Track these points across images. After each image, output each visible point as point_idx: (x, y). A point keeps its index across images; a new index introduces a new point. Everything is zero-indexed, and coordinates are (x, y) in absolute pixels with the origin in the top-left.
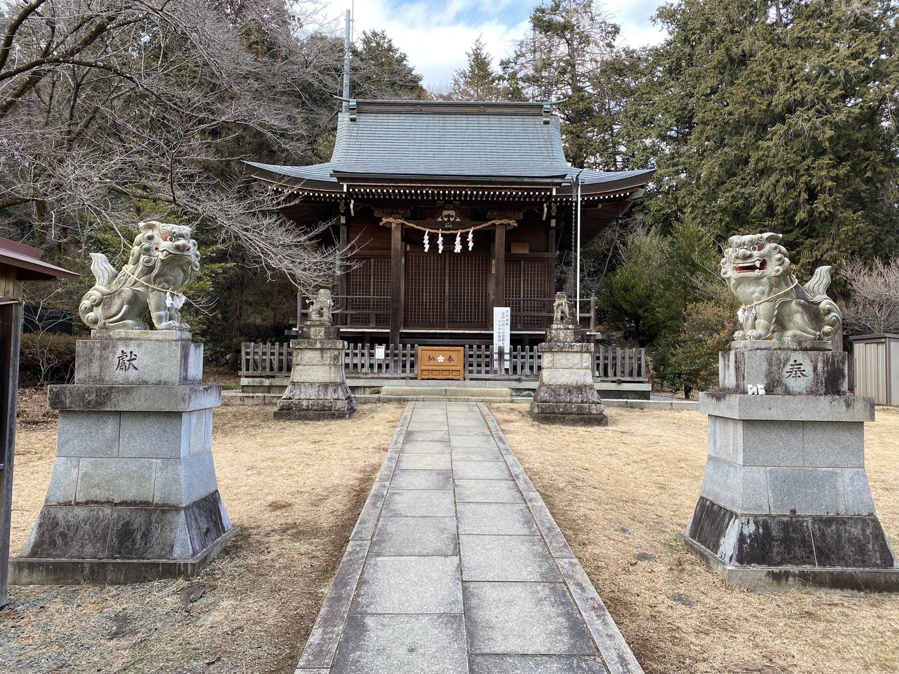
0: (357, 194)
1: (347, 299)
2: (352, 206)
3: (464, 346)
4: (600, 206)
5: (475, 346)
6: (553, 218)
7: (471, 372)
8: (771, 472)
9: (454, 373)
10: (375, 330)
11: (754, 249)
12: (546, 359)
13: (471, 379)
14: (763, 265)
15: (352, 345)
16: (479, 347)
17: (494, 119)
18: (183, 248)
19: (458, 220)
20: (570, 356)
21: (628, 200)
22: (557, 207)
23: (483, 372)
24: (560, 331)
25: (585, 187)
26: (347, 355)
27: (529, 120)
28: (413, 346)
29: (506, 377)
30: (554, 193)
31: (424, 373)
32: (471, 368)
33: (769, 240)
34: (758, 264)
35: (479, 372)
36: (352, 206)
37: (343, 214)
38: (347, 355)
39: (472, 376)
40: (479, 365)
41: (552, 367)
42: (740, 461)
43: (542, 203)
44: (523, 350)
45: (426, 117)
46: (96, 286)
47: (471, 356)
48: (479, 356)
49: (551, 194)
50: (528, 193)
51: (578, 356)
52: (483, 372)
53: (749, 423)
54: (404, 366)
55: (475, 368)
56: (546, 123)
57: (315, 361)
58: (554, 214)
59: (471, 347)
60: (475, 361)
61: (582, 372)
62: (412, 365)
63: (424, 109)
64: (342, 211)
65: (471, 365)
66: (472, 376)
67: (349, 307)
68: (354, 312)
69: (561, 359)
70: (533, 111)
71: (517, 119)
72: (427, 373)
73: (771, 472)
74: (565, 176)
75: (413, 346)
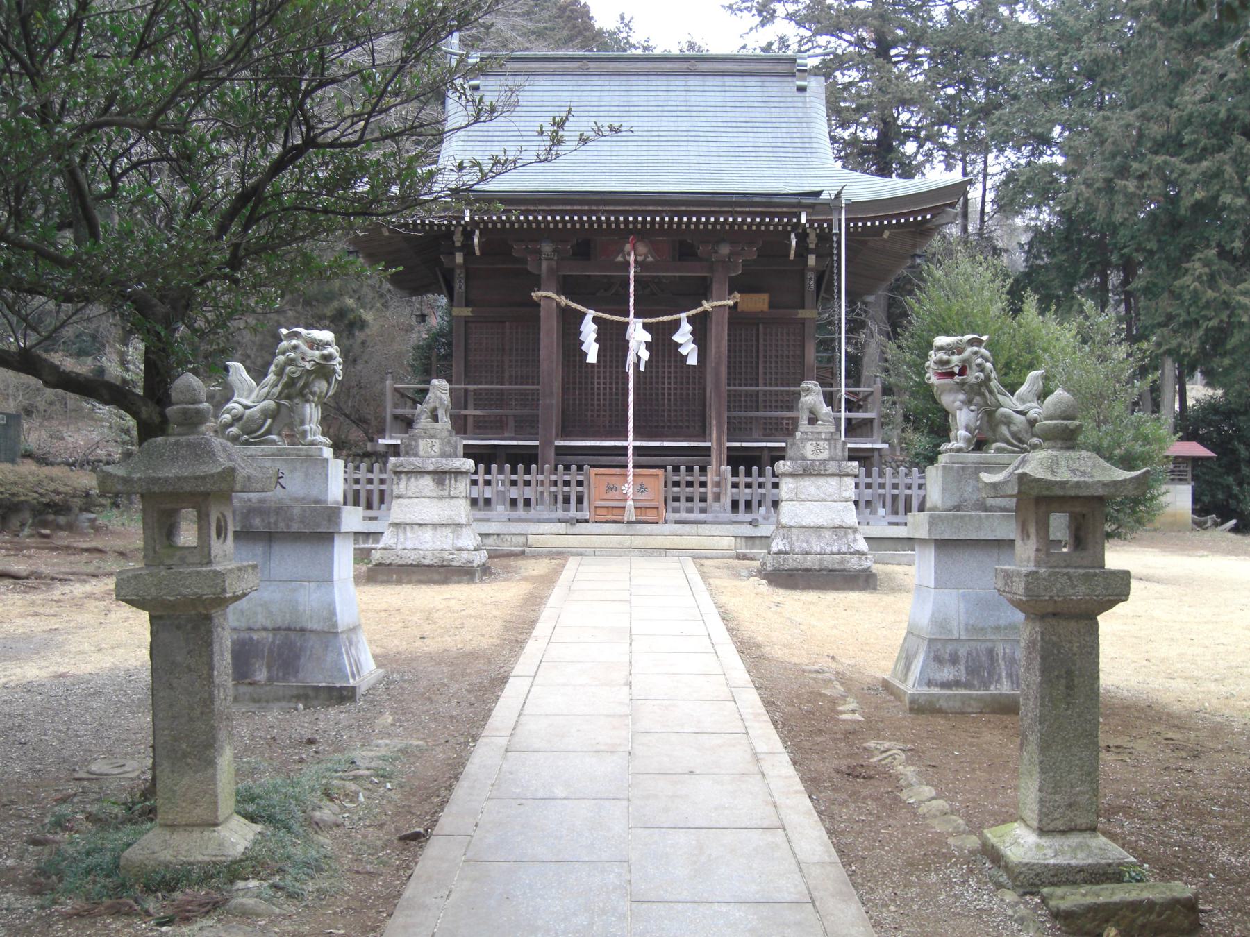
0: (485, 223)
1: (466, 391)
2: (476, 241)
3: (664, 467)
4: (886, 234)
5: (683, 468)
6: (811, 252)
7: (676, 510)
8: (964, 595)
9: (649, 512)
10: (514, 443)
11: (953, 354)
12: (787, 486)
13: (677, 522)
14: (963, 371)
15: (481, 467)
16: (690, 469)
17: (712, 84)
18: (329, 357)
19: (650, 259)
20: (821, 481)
21: (929, 225)
22: (817, 235)
23: (696, 509)
24: (813, 444)
25: (852, 206)
26: (474, 482)
27: (773, 84)
28: (580, 468)
29: (733, 517)
30: (803, 220)
31: (600, 511)
32: (676, 504)
33: (971, 342)
34: (957, 370)
35: (690, 510)
36: (476, 241)
37: (460, 249)
38: (474, 482)
39: (677, 516)
40: (690, 499)
41: (797, 499)
42: (932, 585)
43: (789, 233)
44: (761, 474)
45: (597, 81)
46: (235, 399)
47: (676, 484)
48: (690, 484)
49: (799, 220)
50: (762, 220)
51: (834, 481)
52: (696, 509)
53: (942, 545)
54: (567, 500)
55: (683, 504)
56: (802, 89)
57: (427, 492)
58: (812, 246)
59: (676, 469)
60: (683, 491)
61: (841, 505)
62: (580, 500)
63: (592, 65)
64: (458, 244)
65: (676, 499)
66: (677, 516)
67: (471, 404)
68: (478, 413)
69: (809, 486)
70: (781, 68)
71: (752, 82)
72: (604, 511)
73: (964, 595)
74: (821, 192)
75: (580, 468)
